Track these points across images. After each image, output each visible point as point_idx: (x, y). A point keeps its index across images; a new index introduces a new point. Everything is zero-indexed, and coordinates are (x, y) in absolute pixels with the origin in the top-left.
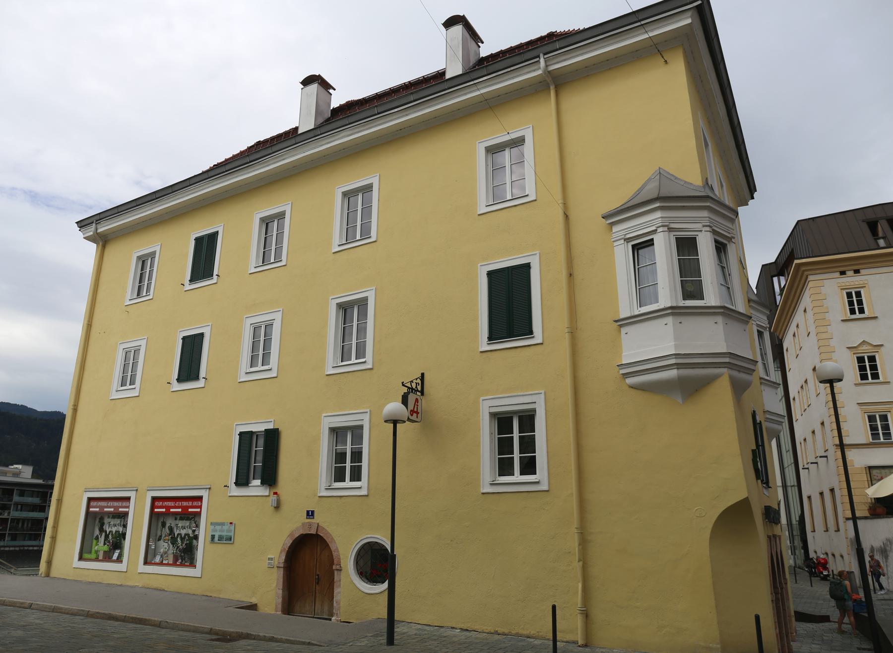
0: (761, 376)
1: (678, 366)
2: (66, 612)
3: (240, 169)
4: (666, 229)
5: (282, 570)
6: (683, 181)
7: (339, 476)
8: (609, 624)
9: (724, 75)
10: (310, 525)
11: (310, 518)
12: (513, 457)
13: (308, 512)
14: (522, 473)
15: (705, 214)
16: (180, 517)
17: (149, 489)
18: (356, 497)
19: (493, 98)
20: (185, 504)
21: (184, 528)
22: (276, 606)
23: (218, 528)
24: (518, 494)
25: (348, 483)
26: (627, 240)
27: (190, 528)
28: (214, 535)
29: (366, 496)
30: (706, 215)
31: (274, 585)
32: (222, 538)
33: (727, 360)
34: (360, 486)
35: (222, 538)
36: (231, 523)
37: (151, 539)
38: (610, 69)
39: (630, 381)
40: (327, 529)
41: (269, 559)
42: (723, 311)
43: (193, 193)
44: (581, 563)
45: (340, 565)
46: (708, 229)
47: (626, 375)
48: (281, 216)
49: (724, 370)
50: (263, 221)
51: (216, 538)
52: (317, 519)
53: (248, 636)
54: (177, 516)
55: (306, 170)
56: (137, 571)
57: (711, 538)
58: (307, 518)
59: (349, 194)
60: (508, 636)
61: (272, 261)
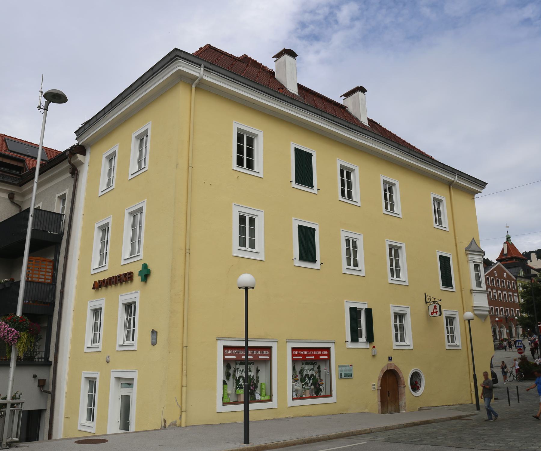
2: (393, 428)
3: (338, 125)
5: (379, 391)
7: (127, 339)
10: (391, 364)
11: (390, 361)
13: (389, 357)
14: (401, 341)
16: (306, 363)
17: (287, 341)
20: (316, 353)
21: (310, 370)
22: (378, 411)
23: (344, 368)
25: (131, 342)
26: (474, 262)
27: (314, 370)
28: (342, 374)
31: (377, 399)
32: (346, 375)
35: (346, 375)
36: (351, 365)
40: (398, 366)
41: (373, 385)
43: (306, 116)
45: (404, 384)
51: (343, 376)
52: (394, 361)
54: (237, 362)
56: (287, 405)
58: (389, 361)
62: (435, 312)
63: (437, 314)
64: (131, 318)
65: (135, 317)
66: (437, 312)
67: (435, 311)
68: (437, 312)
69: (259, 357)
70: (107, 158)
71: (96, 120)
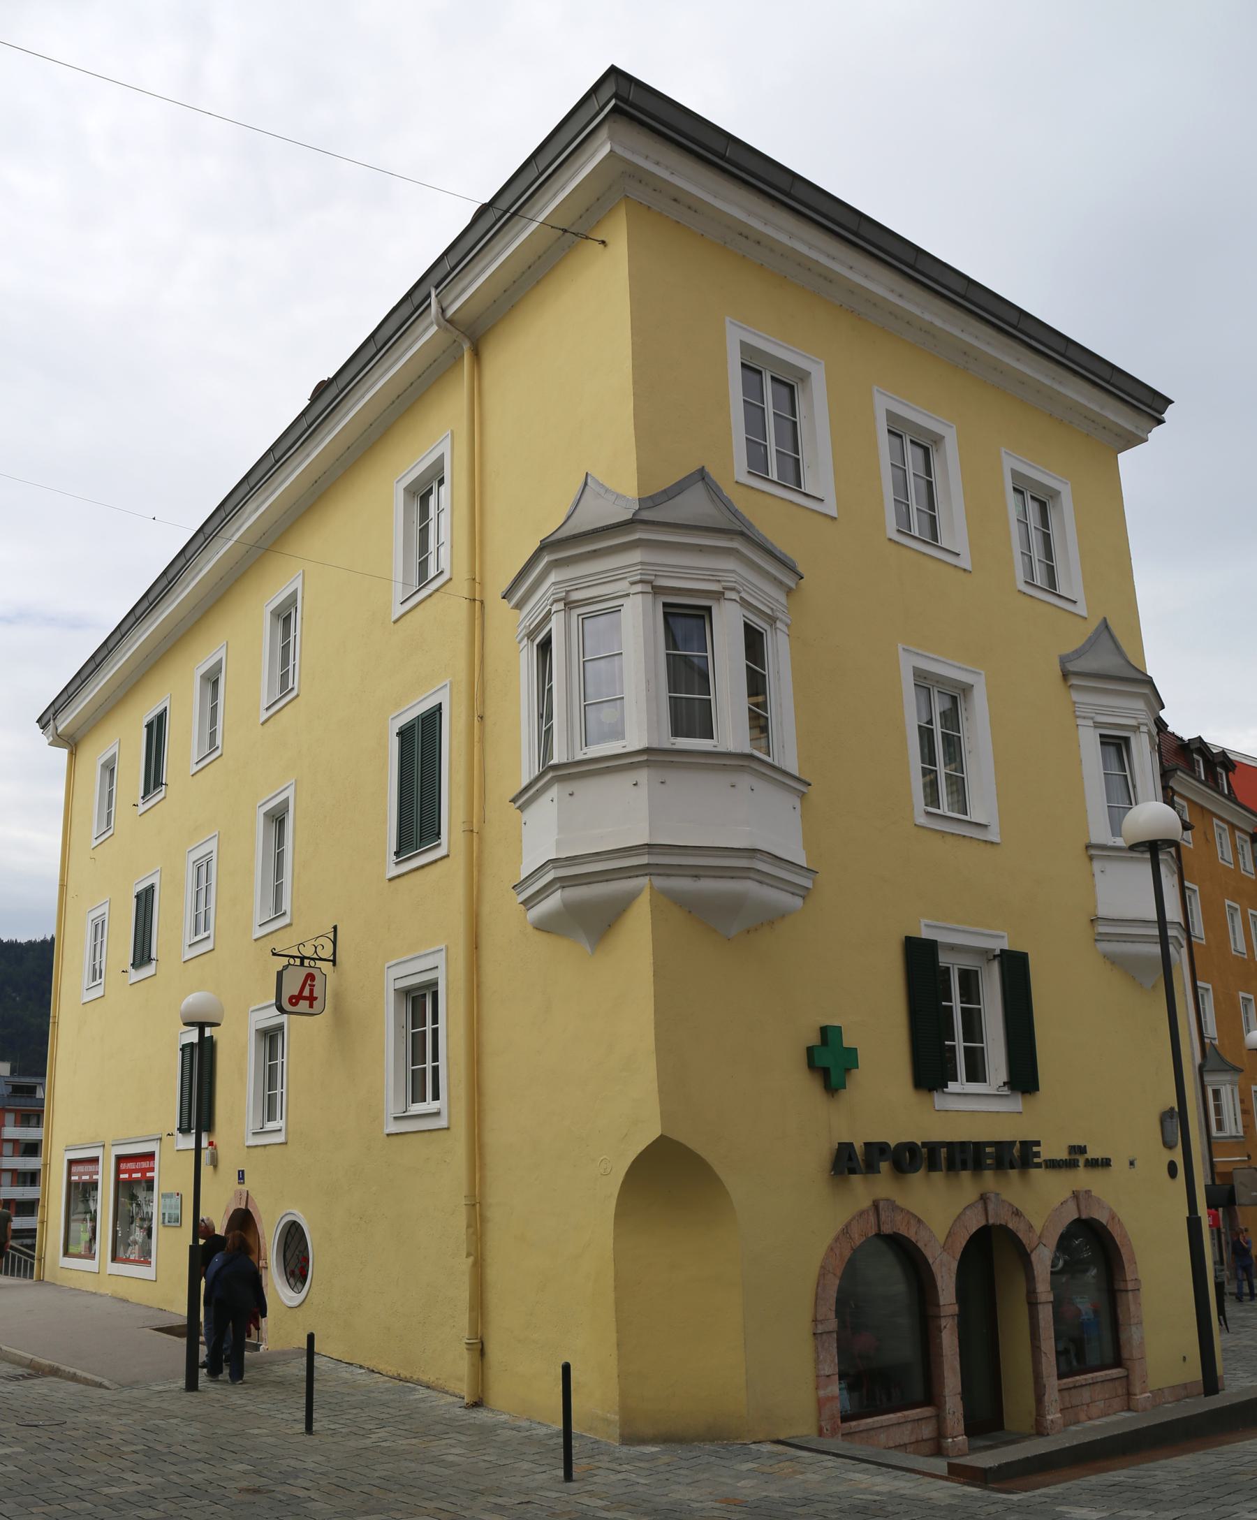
0: (1095, 840)
1: (563, 882)
4: (649, 589)
6: (614, 493)
7: (419, 1096)
8: (506, 1370)
9: (826, 207)
15: (636, 556)
18: (276, 1146)
19: (405, 391)
24: (419, 1135)
25: (429, 1106)
26: (1097, 725)
29: (445, 1129)
30: (639, 560)
33: (644, 860)
34: (279, 1128)
38: (538, 282)
42: (645, 758)
44: (471, 1259)
46: (639, 588)
49: (644, 881)
53: (54, 1372)
55: (236, 581)
57: (618, 1216)
59: (282, 612)
60: (408, 1384)
62: (305, 998)
63: (311, 1006)
64: (425, 1030)
65: (437, 1028)
66: (316, 998)
67: (306, 993)
68: (316, 998)
69: (987, 1149)
70: (276, 614)
71: (203, 539)
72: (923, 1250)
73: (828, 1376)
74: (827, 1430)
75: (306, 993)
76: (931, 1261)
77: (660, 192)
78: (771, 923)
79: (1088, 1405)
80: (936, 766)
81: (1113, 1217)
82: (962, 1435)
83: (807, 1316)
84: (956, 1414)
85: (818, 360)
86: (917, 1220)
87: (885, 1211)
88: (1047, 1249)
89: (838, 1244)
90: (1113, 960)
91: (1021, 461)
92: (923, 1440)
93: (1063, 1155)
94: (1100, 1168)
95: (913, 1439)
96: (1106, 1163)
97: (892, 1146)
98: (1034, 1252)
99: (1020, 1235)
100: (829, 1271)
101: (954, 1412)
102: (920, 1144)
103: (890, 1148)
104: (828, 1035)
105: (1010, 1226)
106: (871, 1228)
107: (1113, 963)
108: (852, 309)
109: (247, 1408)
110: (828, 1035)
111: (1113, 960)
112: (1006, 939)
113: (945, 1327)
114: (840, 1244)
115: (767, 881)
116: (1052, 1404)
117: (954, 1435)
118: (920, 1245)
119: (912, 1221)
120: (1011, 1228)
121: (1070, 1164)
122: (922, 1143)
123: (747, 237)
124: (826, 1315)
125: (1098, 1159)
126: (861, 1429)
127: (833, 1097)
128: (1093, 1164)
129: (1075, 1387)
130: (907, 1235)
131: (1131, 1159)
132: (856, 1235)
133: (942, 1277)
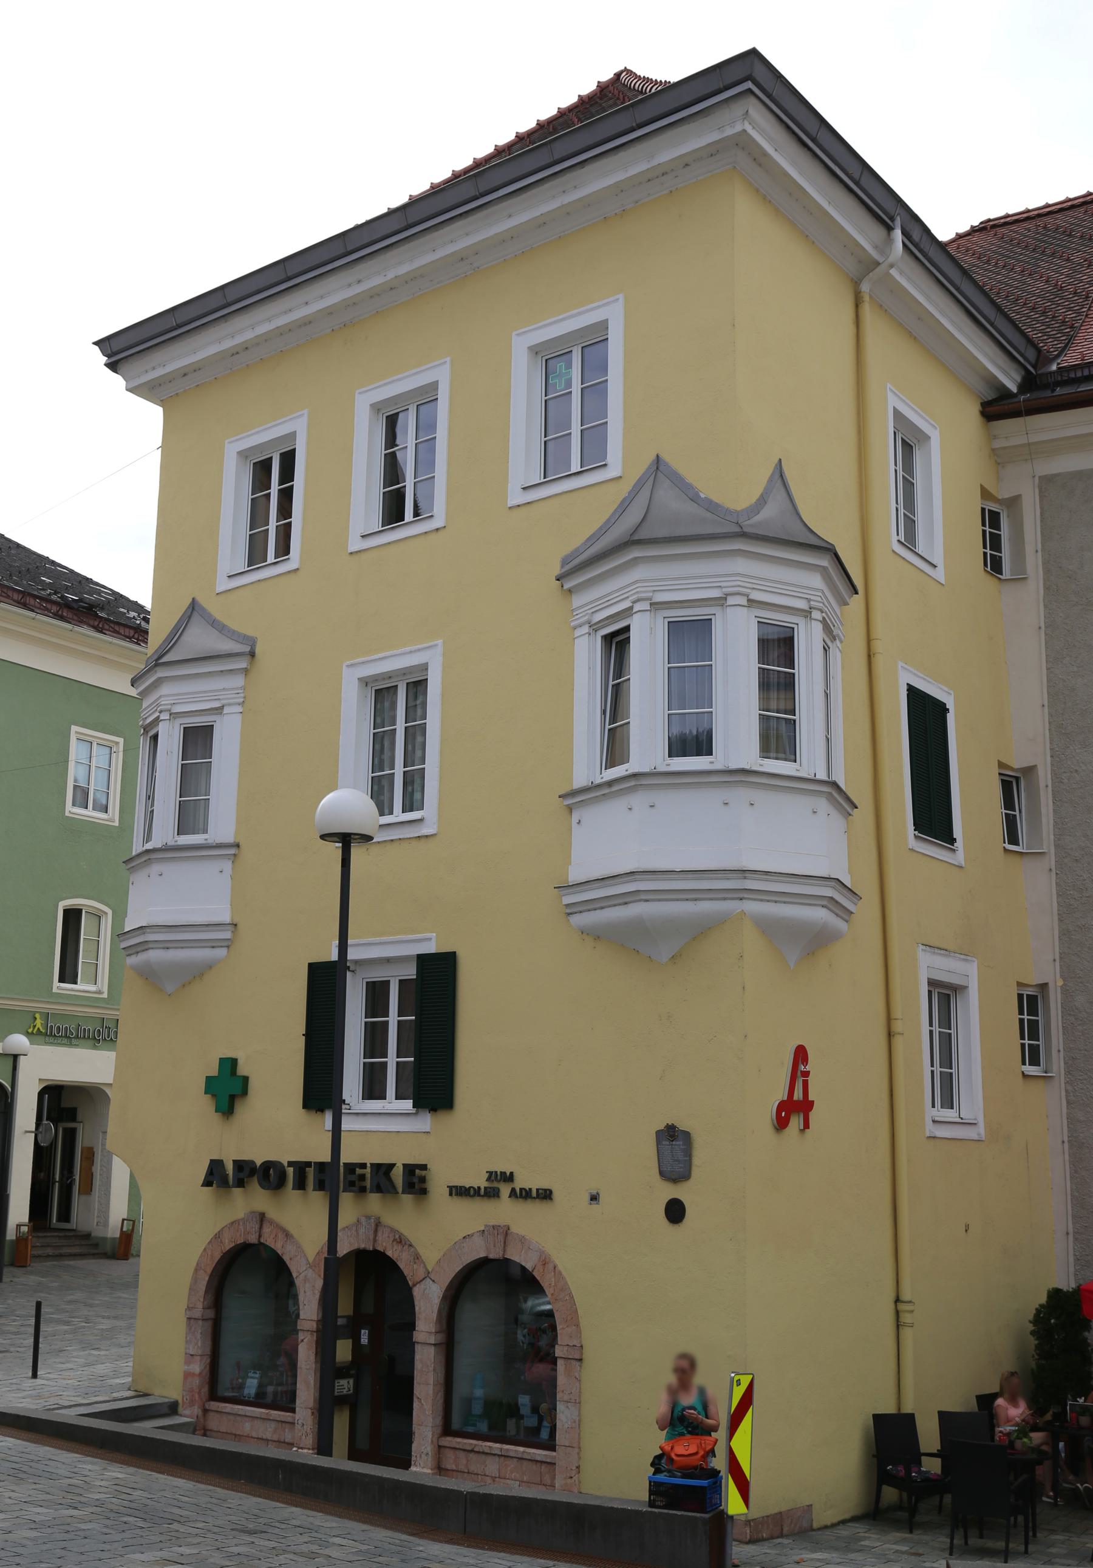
12: (386, 1062)
26: (595, 627)
33: (828, 892)
37: (954, 1550)
39: (578, 920)
47: (572, 910)
48: (427, 396)
50: (247, 457)
61: (574, 470)
67: (798, 1095)
72: (288, 1263)
73: (192, 1355)
74: (187, 1399)
75: (798, 1095)
76: (294, 1275)
77: (174, 379)
78: (202, 975)
79: (494, 1479)
80: (1001, 553)
81: (545, 1261)
82: (309, 1449)
83: (184, 1304)
84: (305, 1427)
85: (299, 414)
86: (285, 1234)
87: (250, 1223)
88: (436, 1285)
89: (210, 1246)
90: (596, 935)
91: (545, 326)
92: (284, 1442)
93: (481, 1182)
94: (492, 1198)
95: (275, 1438)
96: (546, 1195)
97: (258, 1163)
98: (418, 1286)
99: (402, 1266)
100: (201, 1268)
101: (303, 1425)
102: (286, 1164)
103: (256, 1166)
104: (230, 1065)
105: (389, 1253)
106: (241, 1235)
107: (597, 938)
108: (343, 324)
109: (273, 1544)
110: (230, 1065)
111: (596, 935)
112: (434, 940)
113: (302, 1341)
114: (212, 1246)
115: (139, 949)
116: (421, 1456)
117: (301, 1446)
118: (286, 1258)
119: (280, 1235)
120: (391, 1256)
121: (492, 1194)
122: (289, 1162)
123: (238, 353)
124: (195, 1305)
125: (530, 1189)
126: (227, 1411)
127: (228, 1119)
128: (525, 1195)
129: (472, 1451)
130: (273, 1247)
131: (594, 1192)
132: (227, 1241)
133: (305, 1292)
